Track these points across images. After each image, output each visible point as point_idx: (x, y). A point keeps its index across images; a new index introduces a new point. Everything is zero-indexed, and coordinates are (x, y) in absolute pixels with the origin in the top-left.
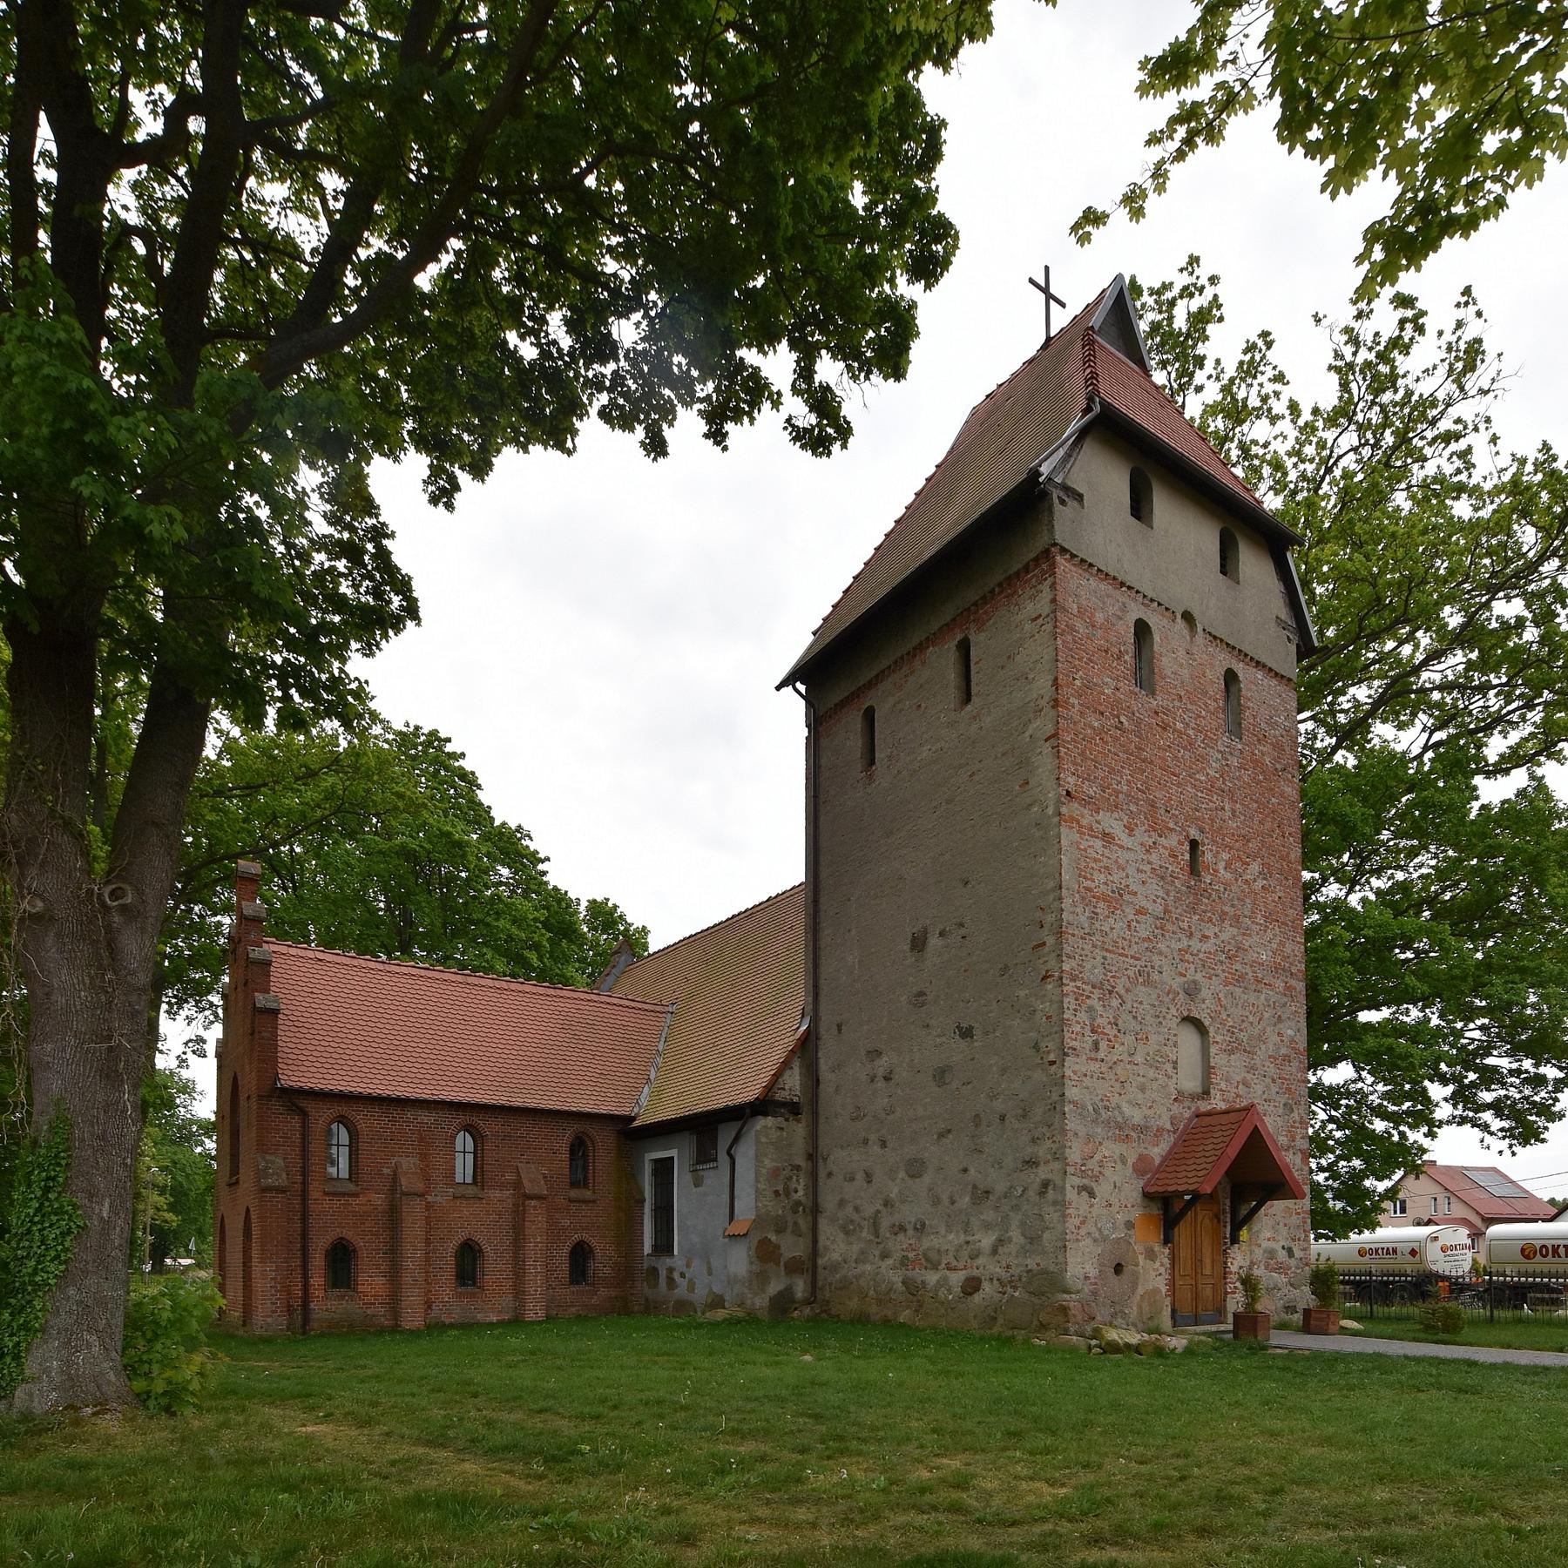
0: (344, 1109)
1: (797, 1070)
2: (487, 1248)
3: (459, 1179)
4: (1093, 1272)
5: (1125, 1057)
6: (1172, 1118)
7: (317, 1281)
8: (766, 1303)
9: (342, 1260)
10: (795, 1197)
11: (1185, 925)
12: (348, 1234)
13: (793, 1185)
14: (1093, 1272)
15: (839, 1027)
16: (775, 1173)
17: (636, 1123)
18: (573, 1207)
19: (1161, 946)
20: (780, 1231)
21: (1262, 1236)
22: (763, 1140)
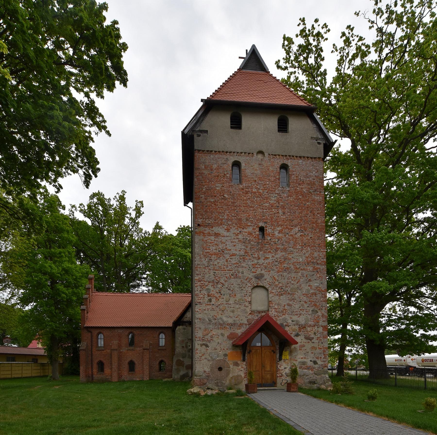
0: (101, 331)
2: (136, 362)
3: (99, 345)
4: (207, 370)
5: (225, 302)
6: (248, 320)
7: (95, 370)
8: (179, 377)
9: (101, 365)
11: (256, 256)
12: (134, 360)
14: (207, 370)
19: (244, 265)
20: (183, 357)
21: (298, 357)
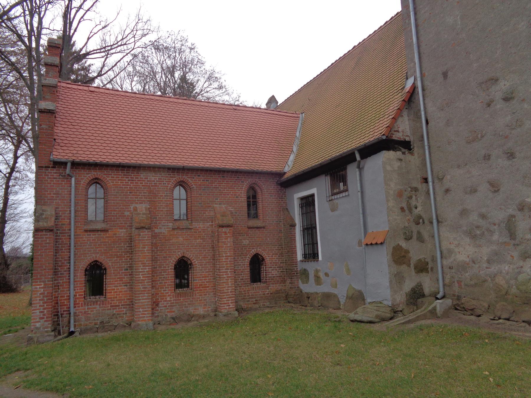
1: (406, 118)
10: (416, 212)
13: (413, 202)
15: (445, 75)
16: (400, 194)
17: (286, 176)
18: (250, 231)
20: (408, 238)
22: (388, 168)
